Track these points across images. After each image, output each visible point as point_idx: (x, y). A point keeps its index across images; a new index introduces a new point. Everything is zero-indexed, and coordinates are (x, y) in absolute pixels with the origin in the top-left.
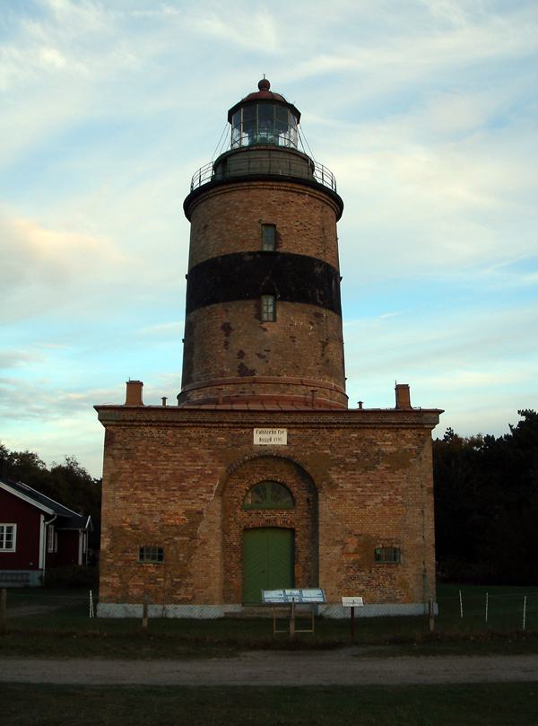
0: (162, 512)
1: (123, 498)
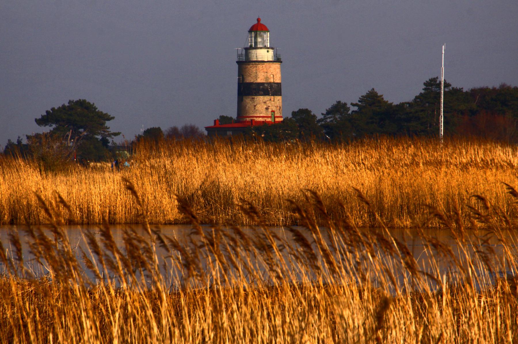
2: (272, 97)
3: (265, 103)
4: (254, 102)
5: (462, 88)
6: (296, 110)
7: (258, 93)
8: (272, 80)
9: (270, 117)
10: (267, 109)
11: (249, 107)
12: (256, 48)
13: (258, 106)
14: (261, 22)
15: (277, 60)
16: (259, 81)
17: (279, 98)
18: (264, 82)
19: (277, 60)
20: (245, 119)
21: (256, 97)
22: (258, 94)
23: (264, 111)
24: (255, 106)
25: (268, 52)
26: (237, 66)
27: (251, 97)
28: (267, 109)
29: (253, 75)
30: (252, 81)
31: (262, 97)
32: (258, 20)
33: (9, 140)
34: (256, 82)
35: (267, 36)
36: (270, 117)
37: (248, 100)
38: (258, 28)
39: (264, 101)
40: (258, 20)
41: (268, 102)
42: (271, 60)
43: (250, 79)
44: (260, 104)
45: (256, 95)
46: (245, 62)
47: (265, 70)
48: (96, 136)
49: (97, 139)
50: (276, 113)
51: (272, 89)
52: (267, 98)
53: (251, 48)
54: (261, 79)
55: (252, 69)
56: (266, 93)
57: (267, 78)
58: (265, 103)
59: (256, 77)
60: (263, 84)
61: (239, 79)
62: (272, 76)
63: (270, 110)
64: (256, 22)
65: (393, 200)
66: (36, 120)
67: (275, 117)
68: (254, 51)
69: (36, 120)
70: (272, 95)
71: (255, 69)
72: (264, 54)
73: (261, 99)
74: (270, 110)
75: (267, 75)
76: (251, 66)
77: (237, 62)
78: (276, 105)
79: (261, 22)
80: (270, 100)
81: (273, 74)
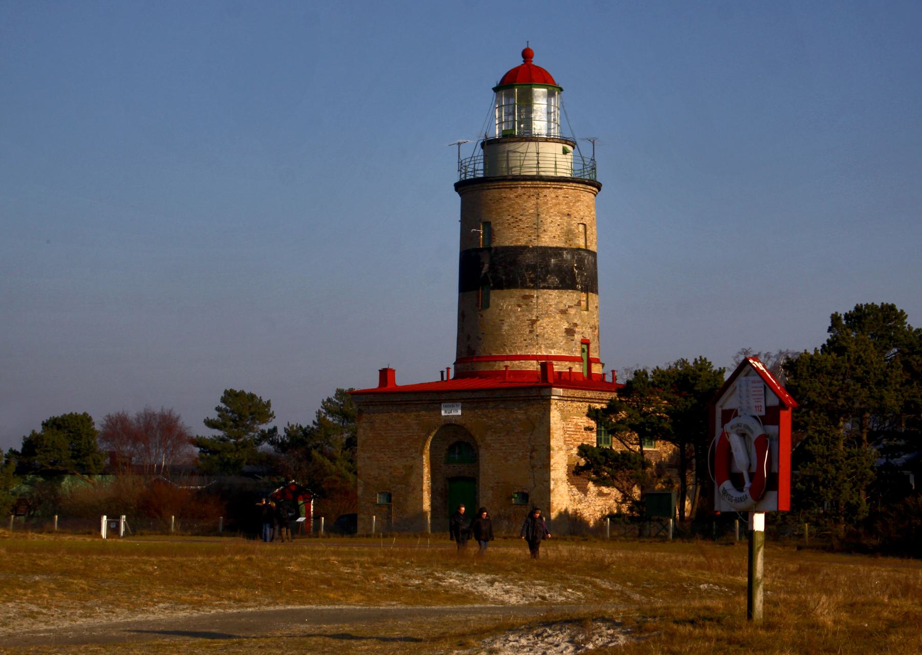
0: (391, 467)
1: (369, 458)
2: (583, 296)
3: (564, 312)
4: (530, 311)
5: (33, 431)
6: (346, 388)
7: (544, 280)
8: (581, 243)
9: (580, 360)
10: (570, 332)
11: (511, 327)
12: (531, 138)
13: (544, 322)
14: (535, 61)
18: (561, 245)
20: (501, 366)
21: (535, 293)
23: (561, 339)
24: (533, 322)
25: (565, 152)
26: (456, 199)
27: (518, 293)
28: (570, 332)
30: (522, 243)
31: (555, 293)
32: (527, 54)
33: (33, 431)
34: (536, 243)
36: (580, 360)
37: (506, 303)
38: (520, 81)
39: (561, 307)
40: (527, 54)
41: (572, 311)
42: (567, 174)
43: (509, 238)
44: (549, 316)
45: (536, 287)
46: (487, 186)
47: (564, 208)
48: (656, 487)
50: (592, 346)
54: (551, 237)
55: (523, 202)
56: (567, 282)
57: (569, 234)
58: (564, 312)
59: (537, 228)
60: (557, 251)
61: (466, 236)
62: (581, 227)
63: (578, 337)
64: (519, 61)
67: (590, 361)
68: (522, 147)
70: (582, 290)
71: (533, 201)
73: (553, 299)
74: (578, 337)
75: (569, 224)
76: (520, 191)
77: (459, 187)
78: (592, 323)
79: (535, 61)
80: (579, 304)
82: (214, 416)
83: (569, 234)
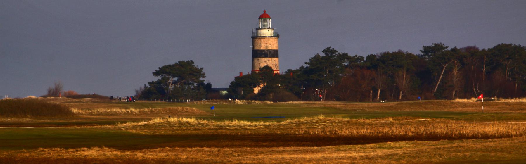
2: (270, 59)
8: (270, 48)
15: (276, 36)
16: (262, 49)
17: (276, 59)
19: (276, 36)
22: (261, 57)
29: (258, 45)
32: (265, 12)
35: (270, 22)
38: (264, 17)
40: (265, 12)
43: (257, 48)
46: (255, 37)
49: (174, 76)
51: (274, 54)
52: (266, 59)
53: (259, 29)
55: (258, 41)
56: (266, 56)
57: (267, 47)
59: (260, 46)
60: (264, 50)
65: (502, 126)
66: (153, 73)
69: (153, 73)
72: (266, 32)
79: (266, 13)
81: (273, 45)
82: (308, 61)
83: (267, 47)
